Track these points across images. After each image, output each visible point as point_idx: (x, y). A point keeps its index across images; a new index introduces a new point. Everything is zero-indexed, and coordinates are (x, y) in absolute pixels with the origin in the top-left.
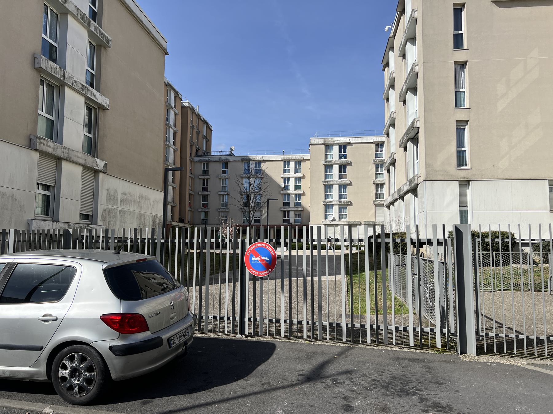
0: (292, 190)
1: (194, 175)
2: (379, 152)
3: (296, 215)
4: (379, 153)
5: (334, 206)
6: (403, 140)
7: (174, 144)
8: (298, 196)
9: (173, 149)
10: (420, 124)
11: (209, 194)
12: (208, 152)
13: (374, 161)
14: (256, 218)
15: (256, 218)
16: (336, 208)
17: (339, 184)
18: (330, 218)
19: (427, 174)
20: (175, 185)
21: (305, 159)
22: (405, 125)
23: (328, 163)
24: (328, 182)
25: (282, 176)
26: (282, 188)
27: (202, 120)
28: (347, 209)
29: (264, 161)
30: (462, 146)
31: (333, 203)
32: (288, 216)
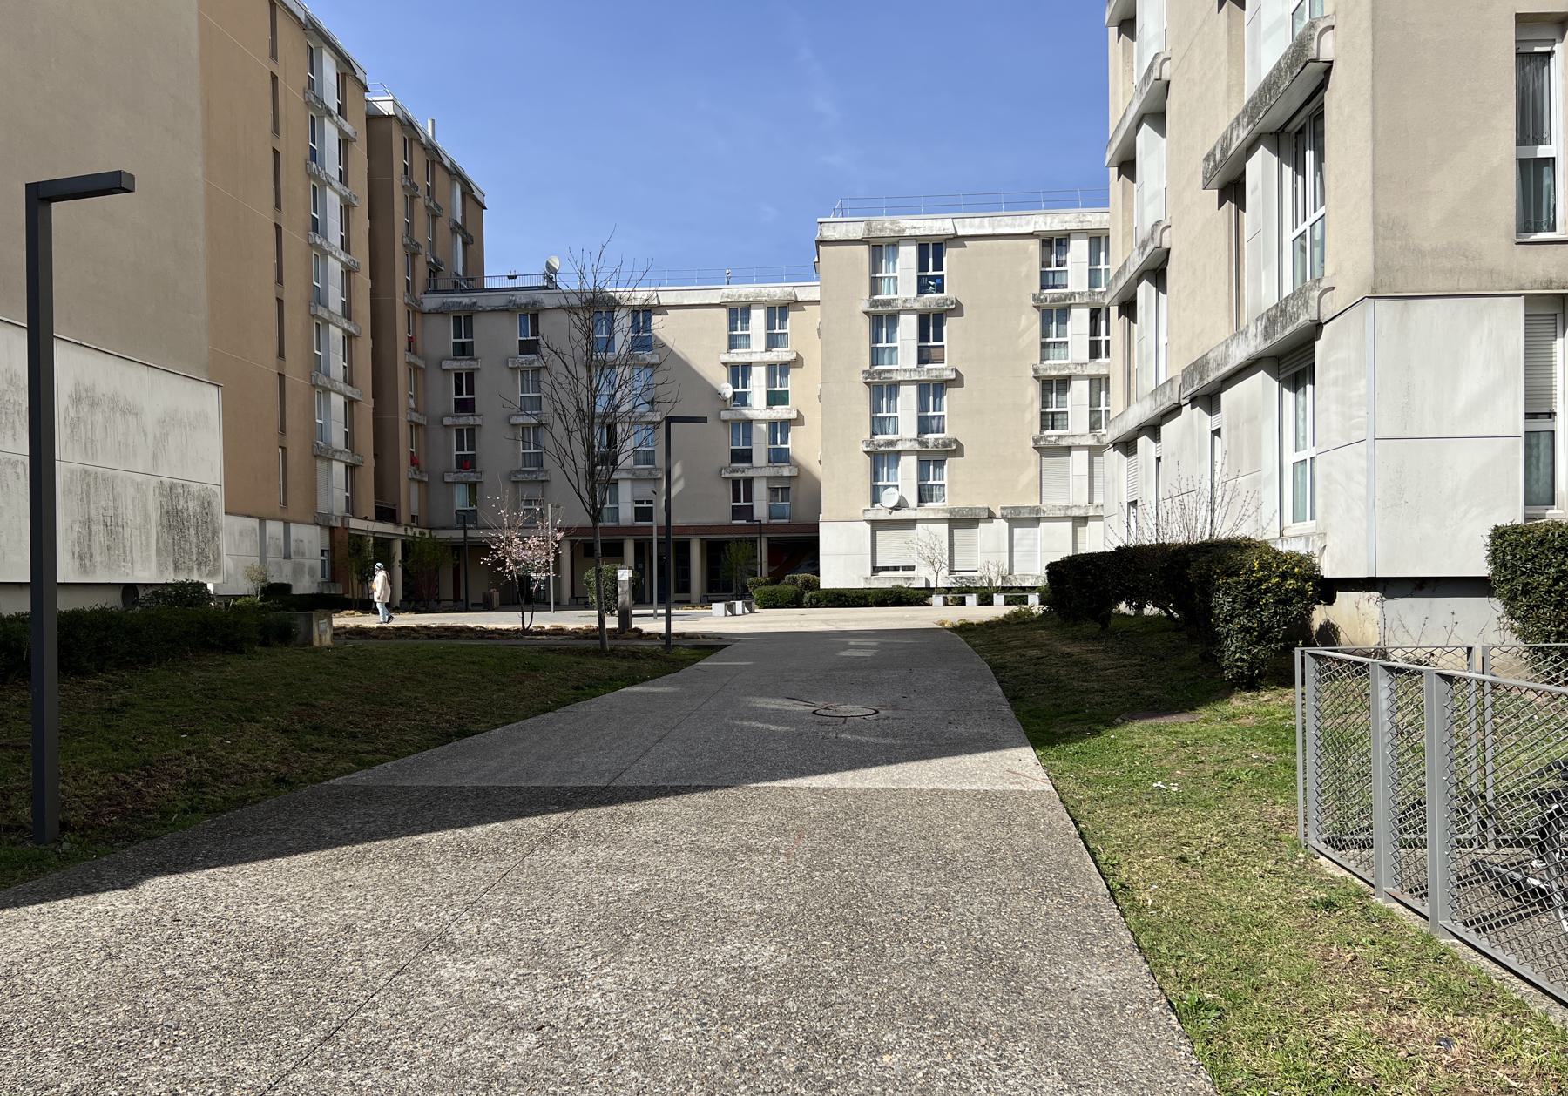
0: (758, 407)
1: (423, 358)
2: (1054, 268)
3: (773, 491)
4: (1054, 272)
5: (903, 458)
6: (1224, 151)
7: (345, 245)
8: (780, 428)
9: (342, 262)
10: (1335, 47)
11: (478, 423)
12: (472, 278)
13: (1036, 298)
14: (642, 502)
15: (642, 502)
16: (909, 464)
17: (917, 381)
18: (889, 498)
19: (1381, 266)
20: (355, 391)
21: (799, 299)
22: (1236, 85)
23: (880, 309)
24: (883, 376)
25: (726, 358)
26: (726, 401)
27: (445, 167)
28: (946, 467)
29: (662, 309)
30: (1535, 133)
31: (899, 447)
32: (749, 497)
